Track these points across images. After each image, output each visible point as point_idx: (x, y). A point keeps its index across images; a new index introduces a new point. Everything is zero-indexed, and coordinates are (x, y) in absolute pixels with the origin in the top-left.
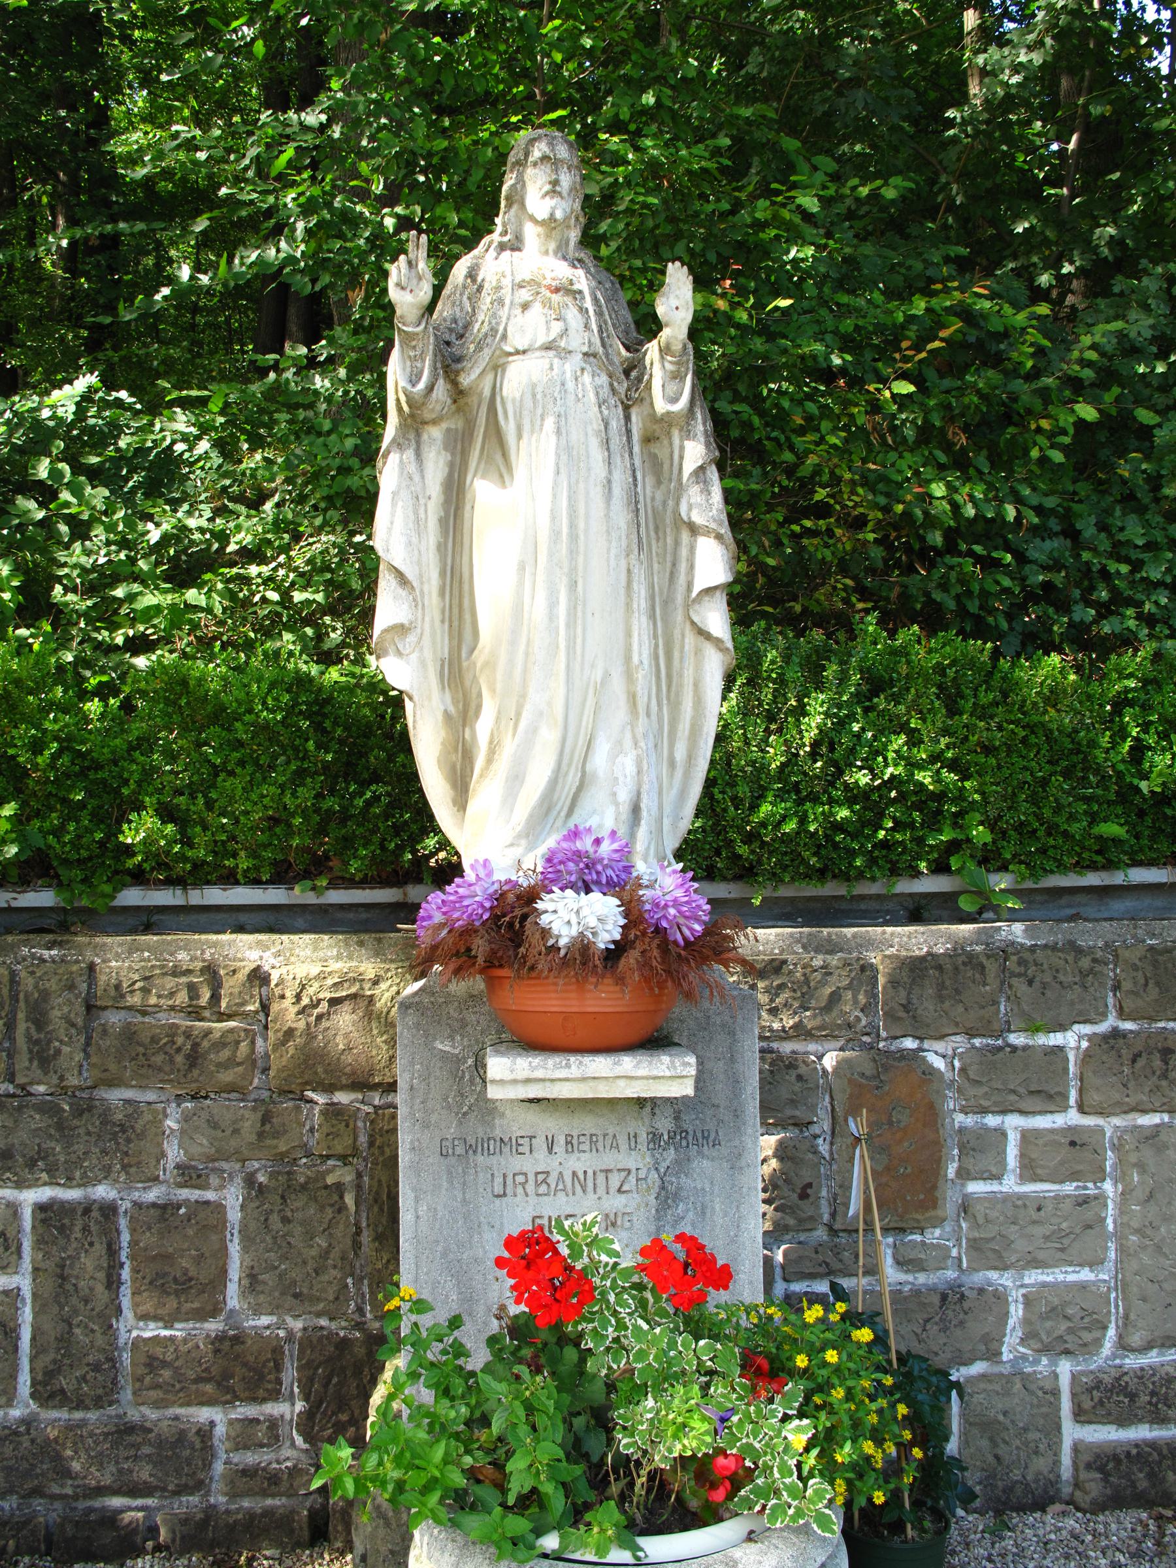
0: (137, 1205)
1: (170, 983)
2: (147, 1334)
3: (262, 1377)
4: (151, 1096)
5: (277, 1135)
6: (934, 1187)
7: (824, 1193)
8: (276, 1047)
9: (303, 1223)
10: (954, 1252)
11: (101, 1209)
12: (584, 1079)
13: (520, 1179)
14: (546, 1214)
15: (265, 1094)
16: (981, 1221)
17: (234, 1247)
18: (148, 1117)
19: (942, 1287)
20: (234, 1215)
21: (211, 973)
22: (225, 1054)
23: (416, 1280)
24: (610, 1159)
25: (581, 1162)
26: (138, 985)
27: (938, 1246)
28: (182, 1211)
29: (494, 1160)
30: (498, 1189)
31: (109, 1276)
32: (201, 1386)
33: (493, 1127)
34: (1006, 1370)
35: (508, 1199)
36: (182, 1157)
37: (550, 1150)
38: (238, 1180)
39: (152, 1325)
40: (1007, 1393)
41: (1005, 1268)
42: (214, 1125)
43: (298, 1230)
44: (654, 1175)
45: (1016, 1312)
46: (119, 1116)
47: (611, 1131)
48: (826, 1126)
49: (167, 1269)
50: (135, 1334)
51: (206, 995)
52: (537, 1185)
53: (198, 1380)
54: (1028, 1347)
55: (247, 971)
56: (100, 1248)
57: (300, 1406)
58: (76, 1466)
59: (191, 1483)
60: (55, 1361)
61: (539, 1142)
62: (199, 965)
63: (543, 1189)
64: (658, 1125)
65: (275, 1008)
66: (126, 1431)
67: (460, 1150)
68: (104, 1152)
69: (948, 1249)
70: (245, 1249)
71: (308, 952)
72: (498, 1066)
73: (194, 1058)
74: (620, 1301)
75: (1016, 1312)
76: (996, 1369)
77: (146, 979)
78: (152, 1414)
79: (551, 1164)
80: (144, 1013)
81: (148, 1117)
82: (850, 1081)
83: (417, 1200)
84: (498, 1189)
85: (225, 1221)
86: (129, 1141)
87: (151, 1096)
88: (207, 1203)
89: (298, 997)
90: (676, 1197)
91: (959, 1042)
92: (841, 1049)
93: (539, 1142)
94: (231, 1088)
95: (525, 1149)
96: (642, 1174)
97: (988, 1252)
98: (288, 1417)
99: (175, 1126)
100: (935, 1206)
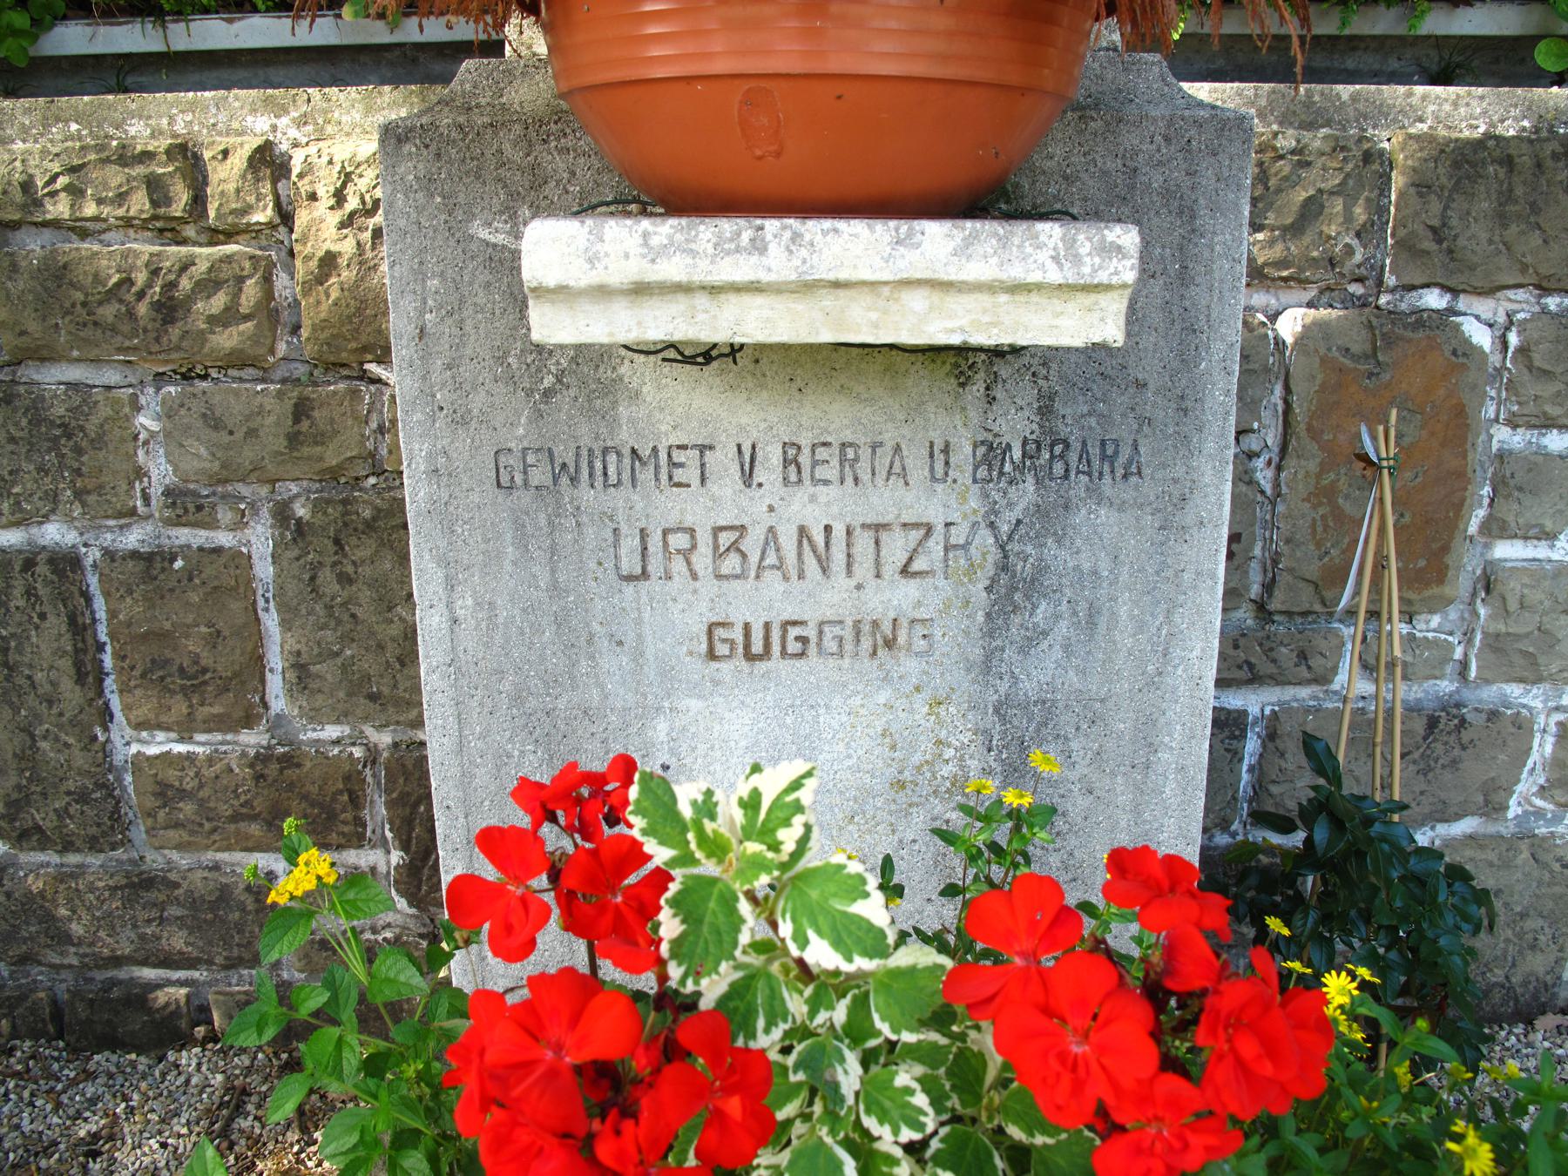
0: (109, 554)
1: (115, 177)
2: (152, 750)
3: (332, 817)
4: (111, 376)
5: (320, 439)
6: (1446, 549)
7: (1257, 551)
8: (308, 288)
9: (373, 584)
10: (1458, 653)
11: (51, 561)
12: (807, 287)
13: (679, 541)
14: (738, 619)
15: (301, 370)
16: (1513, 605)
17: (271, 622)
18: (104, 411)
19: (1429, 705)
20: (264, 570)
21: (187, 156)
22: (219, 302)
23: (461, 747)
24: (884, 500)
25: (815, 507)
26: (62, 181)
27: (1436, 642)
28: (179, 564)
29: (617, 499)
30: (630, 564)
31: (78, 665)
32: (242, 825)
33: (614, 424)
34: (1507, 829)
35: (654, 585)
36: (171, 479)
37: (748, 477)
38: (265, 513)
39: (161, 736)
40: (1506, 864)
41: (1538, 680)
42: (214, 422)
43: (365, 595)
44: (985, 538)
45: (1543, 747)
46: (60, 411)
47: (889, 437)
48: (1272, 438)
49: (168, 654)
50: (134, 748)
51: (181, 198)
52: (718, 555)
53: (236, 818)
54: (1552, 799)
55: (246, 151)
56: (56, 623)
57: (396, 857)
58: (77, 929)
59: (247, 956)
60: (19, 787)
61: (723, 460)
62: (164, 143)
63: (731, 563)
64: (1001, 426)
65: (302, 218)
66: (141, 885)
67: (539, 476)
68: (41, 469)
69: (1450, 647)
70: (286, 625)
71: (357, 115)
72: (552, 248)
73: (170, 309)
74: (876, 1096)
75: (1543, 747)
76: (1492, 829)
77: (73, 170)
78: (183, 860)
79: (752, 509)
80: (84, 234)
81: (104, 411)
82: (1323, 361)
83: (450, 585)
84: (630, 564)
85: (250, 581)
86: (79, 451)
87: (111, 376)
88: (218, 550)
89: (340, 197)
90: (1034, 586)
91: (1522, 302)
92: (1310, 305)
93: (723, 460)
94: (237, 361)
95: (690, 474)
96: (959, 535)
97: (1518, 656)
98: (382, 868)
99: (154, 426)
100: (1441, 578)
